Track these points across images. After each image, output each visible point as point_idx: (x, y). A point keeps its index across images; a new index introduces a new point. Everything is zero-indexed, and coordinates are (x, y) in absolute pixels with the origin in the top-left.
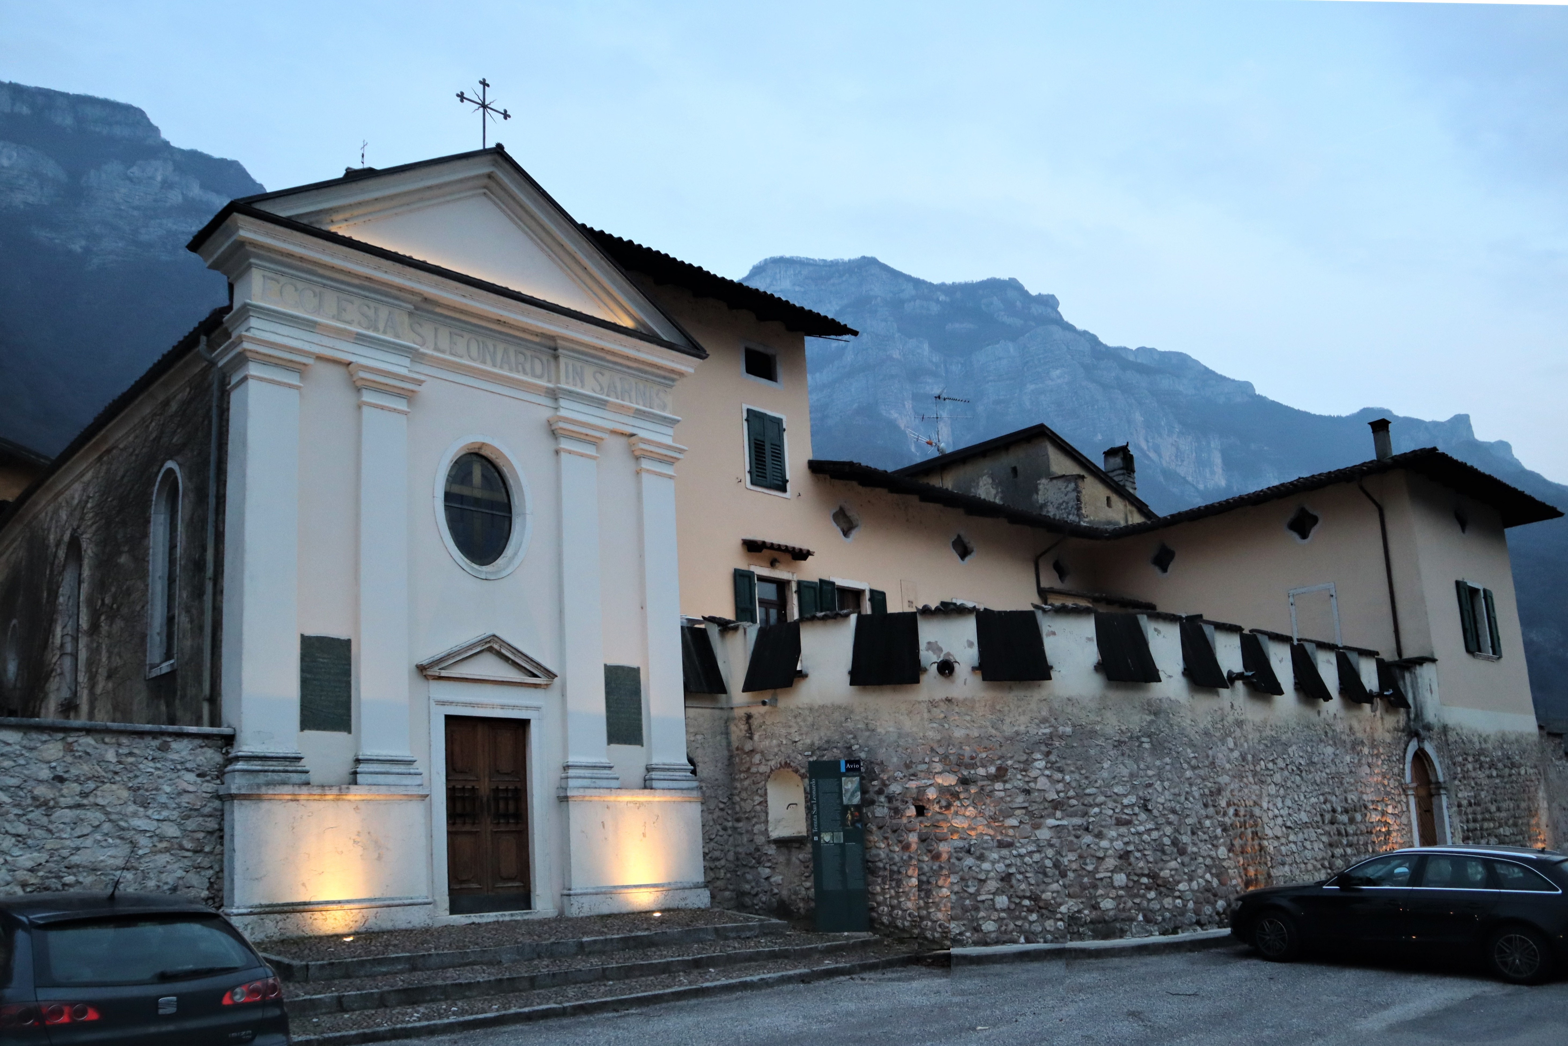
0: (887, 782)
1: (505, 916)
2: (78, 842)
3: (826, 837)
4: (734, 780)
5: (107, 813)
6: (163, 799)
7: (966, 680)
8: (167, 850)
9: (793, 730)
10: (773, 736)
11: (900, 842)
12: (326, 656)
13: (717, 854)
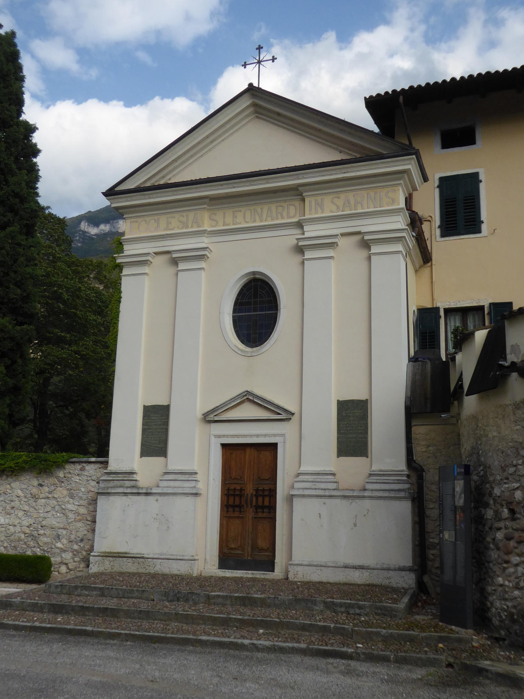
1: (259, 574)
5: (58, 501)
6: (81, 494)
8: (80, 520)
12: (155, 415)
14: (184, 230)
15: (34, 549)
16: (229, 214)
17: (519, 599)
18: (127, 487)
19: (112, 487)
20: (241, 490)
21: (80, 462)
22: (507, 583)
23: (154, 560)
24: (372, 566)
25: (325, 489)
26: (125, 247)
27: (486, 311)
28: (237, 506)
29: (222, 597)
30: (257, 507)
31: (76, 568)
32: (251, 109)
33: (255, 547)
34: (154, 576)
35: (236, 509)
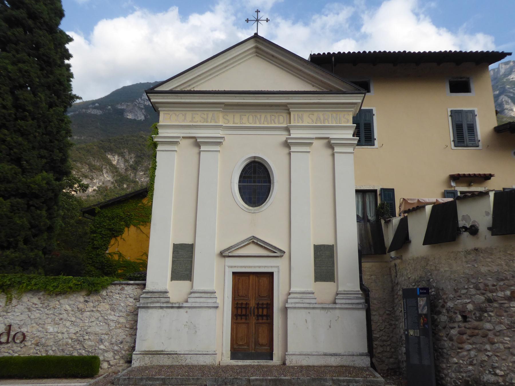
0: (446, 301)
2: (90, 324)
3: (411, 333)
4: (287, 302)
5: (101, 314)
6: (120, 308)
7: (486, 236)
8: (120, 327)
13: (385, 338)
15: (80, 351)
16: (237, 116)
17: (473, 372)
18: (163, 303)
19: (150, 303)
20: (246, 304)
21: (120, 284)
22: (461, 362)
23: (185, 355)
24: (342, 354)
25: (310, 303)
26: (160, 131)
27: (378, 193)
28: (244, 315)
29: (260, 380)
30: (258, 316)
31: (116, 364)
32: (254, 50)
33: (257, 343)
34: (181, 367)
35: (243, 317)
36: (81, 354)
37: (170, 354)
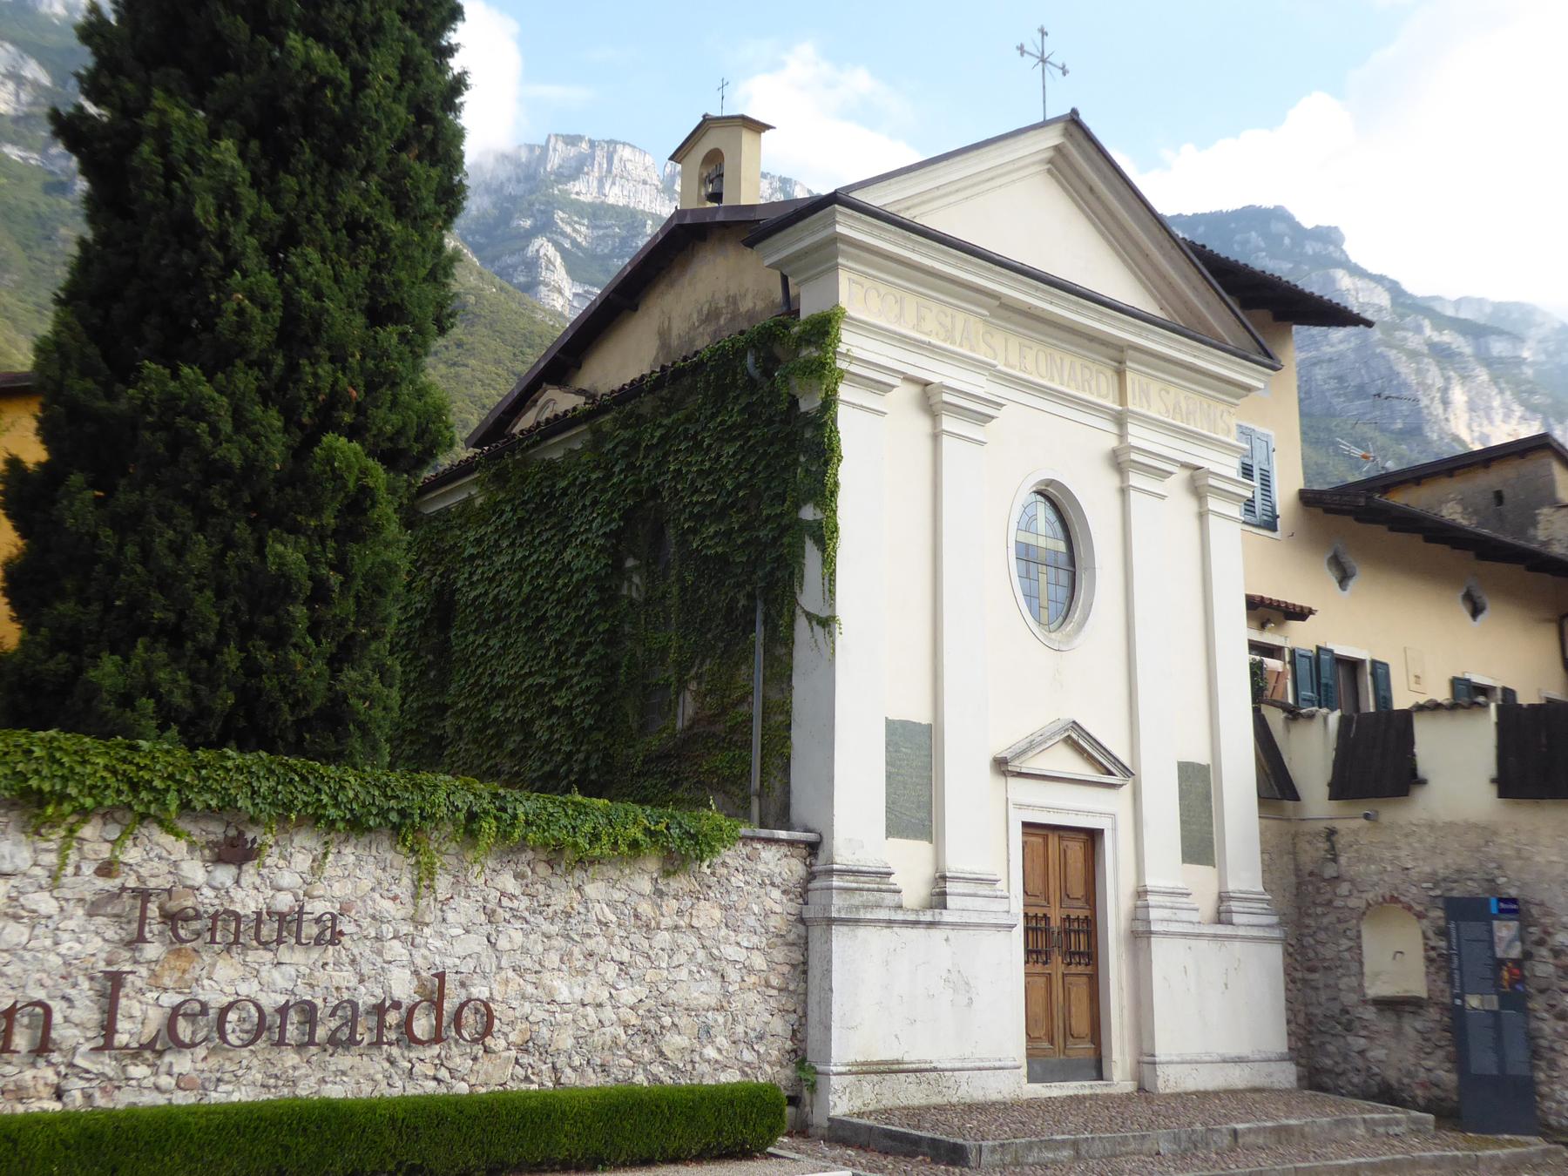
3: (1473, 1001)
9: (1403, 853)
10: (1371, 860)
11: (1553, 1006)
14: (947, 345)
21: (747, 840)
32: (1050, 154)
36: (657, 1079)
37: (921, 1071)
